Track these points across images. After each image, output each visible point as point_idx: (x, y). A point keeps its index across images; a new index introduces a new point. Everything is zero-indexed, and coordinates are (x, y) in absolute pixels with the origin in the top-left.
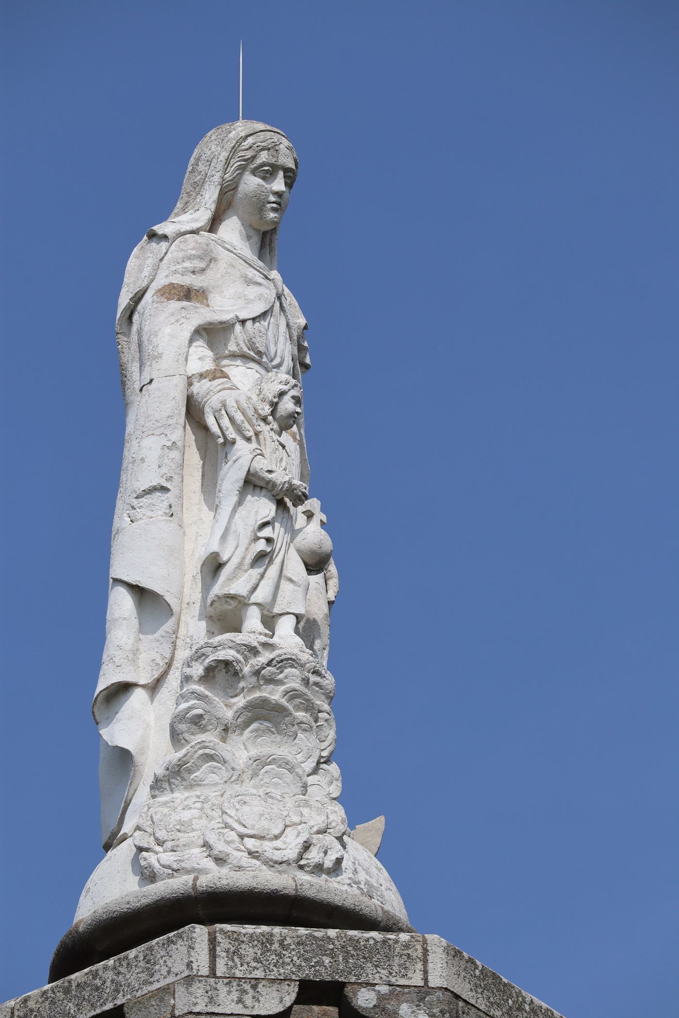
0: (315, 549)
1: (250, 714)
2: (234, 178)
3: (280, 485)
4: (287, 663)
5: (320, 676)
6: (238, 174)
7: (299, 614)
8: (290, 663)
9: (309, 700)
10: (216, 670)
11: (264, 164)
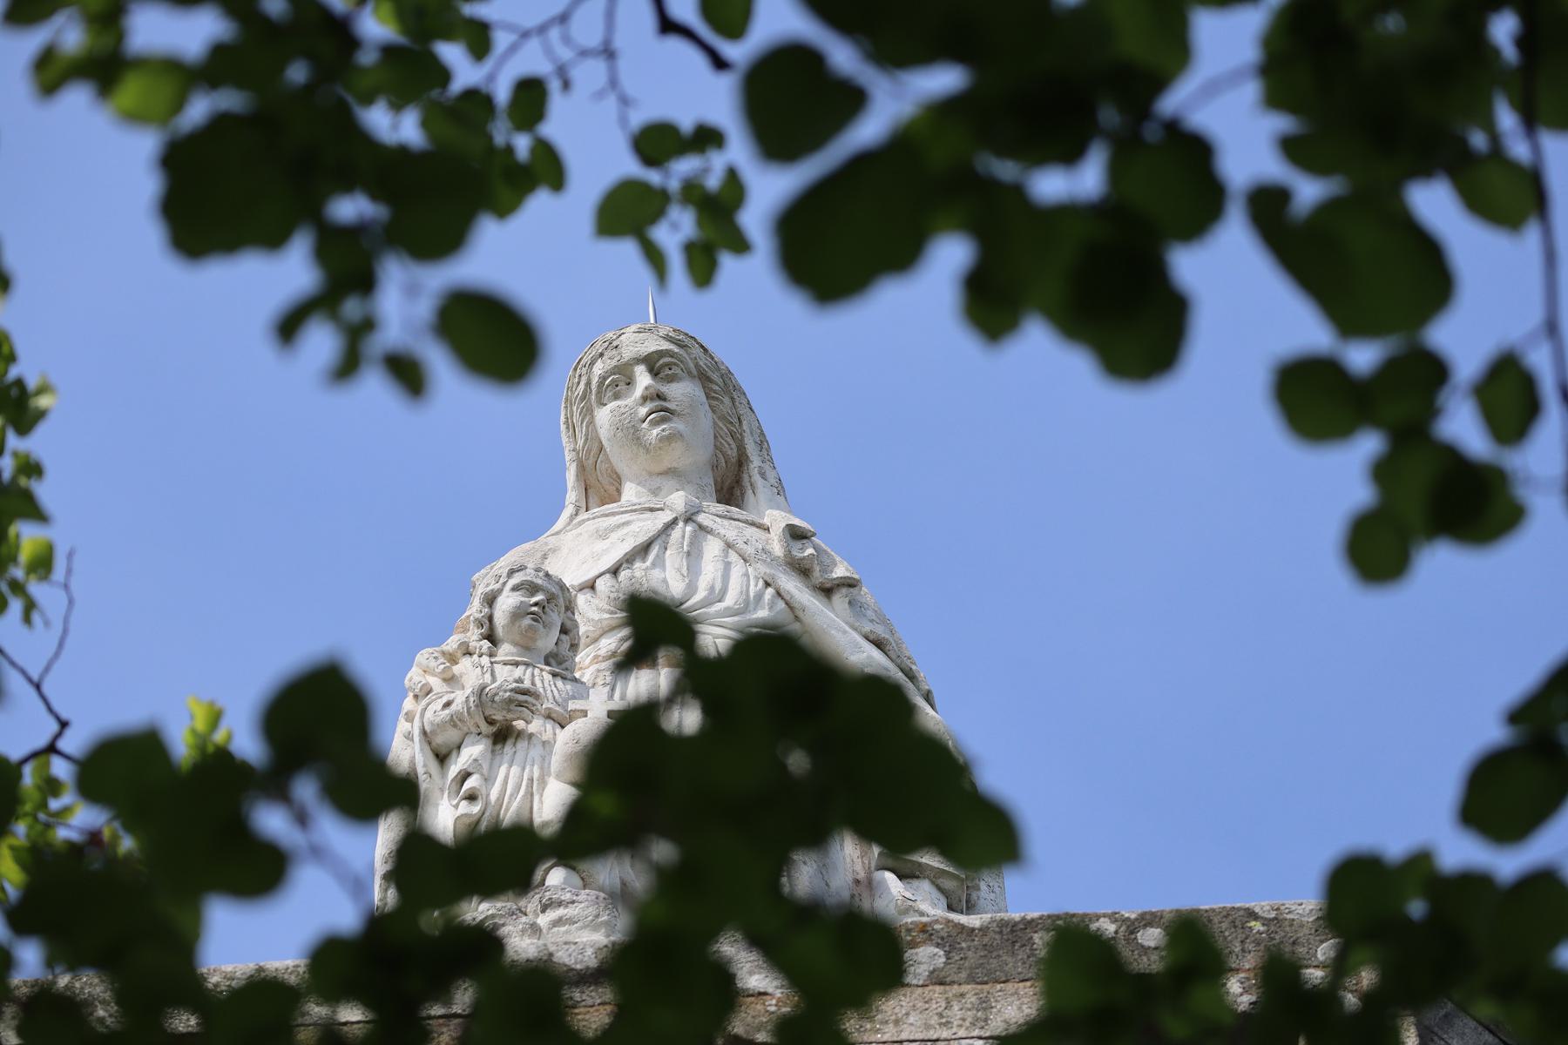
5: (560, 906)
11: (603, 378)
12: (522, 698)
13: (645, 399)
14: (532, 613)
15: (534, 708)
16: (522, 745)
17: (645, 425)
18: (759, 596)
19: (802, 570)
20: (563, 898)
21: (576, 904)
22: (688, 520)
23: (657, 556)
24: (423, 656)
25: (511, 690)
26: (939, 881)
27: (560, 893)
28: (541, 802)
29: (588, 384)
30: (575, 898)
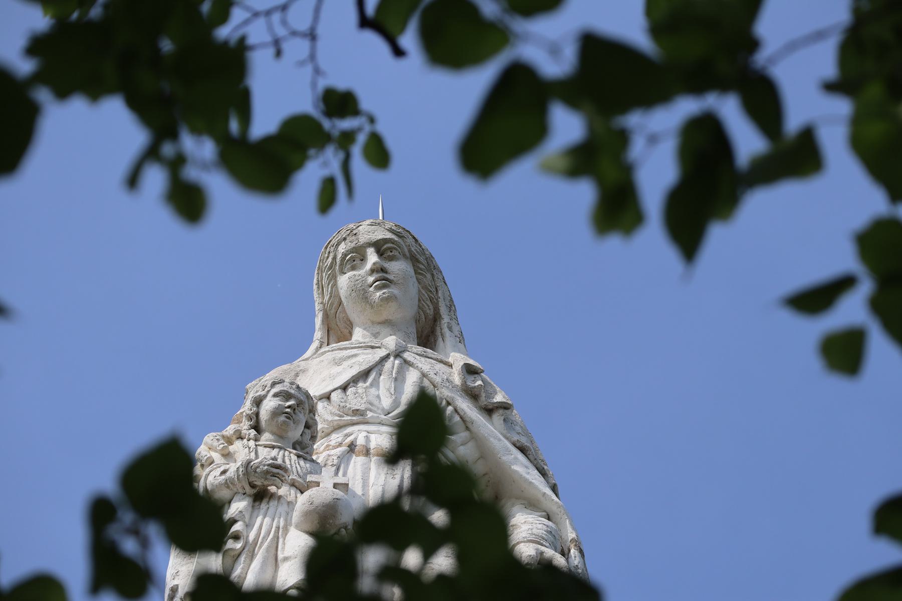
0: (306, 509)
2: (331, 293)
3: (234, 475)
6: (332, 288)
11: (345, 255)
13: (372, 271)
14: (286, 413)
15: (283, 478)
16: (273, 503)
17: (371, 289)
22: (397, 356)
25: (268, 465)
29: (335, 258)
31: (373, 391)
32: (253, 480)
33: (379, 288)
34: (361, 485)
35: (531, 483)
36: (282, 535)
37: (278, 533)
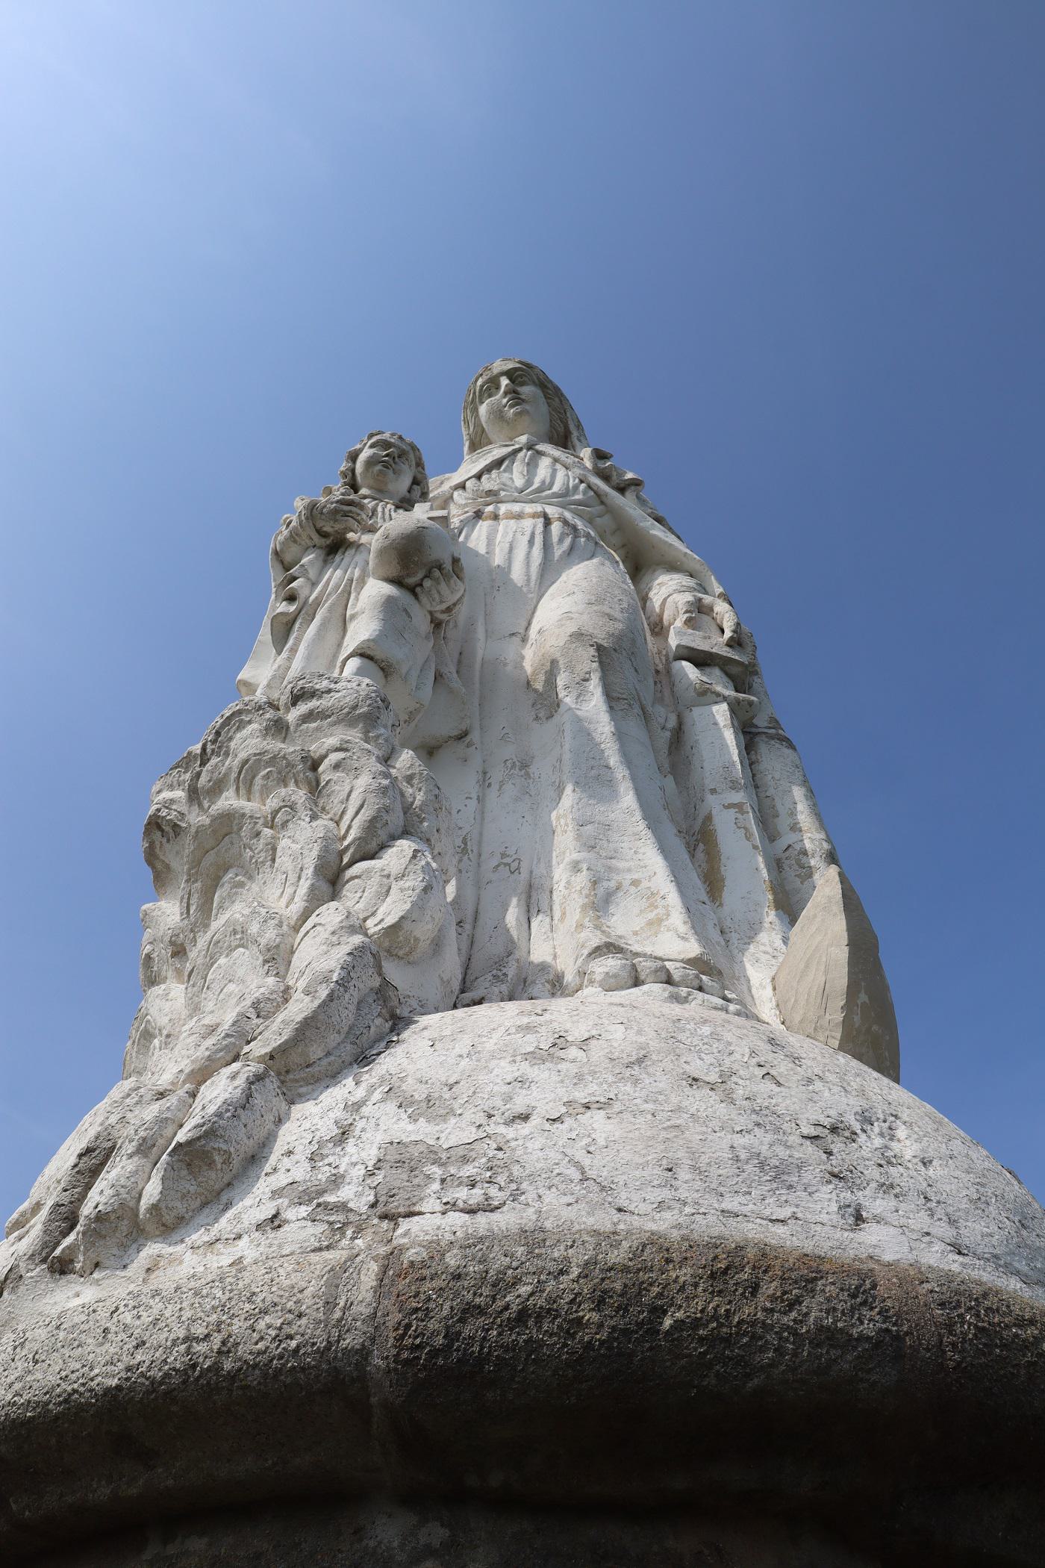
1: (198, 885)
4: (229, 729)
5: (313, 697)
7: (357, 648)
8: (235, 724)
9: (275, 757)
10: (157, 850)
11: (482, 386)
12: (346, 508)
13: (506, 393)
14: (383, 462)
15: (359, 518)
16: (350, 552)
17: (506, 409)
18: (576, 488)
19: (605, 476)
20: (317, 687)
21: (332, 694)
22: (529, 449)
23: (507, 466)
24: (297, 499)
25: (337, 502)
26: (727, 668)
27: (316, 681)
28: (357, 599)
29: (474, 393)
30: (331, 687)
31: (506, 475)
32: (321, 525)
33: (512, 406)
34: (485, 543)
35: (671, 544)
36: (356, 588)
37: (351, 587)
